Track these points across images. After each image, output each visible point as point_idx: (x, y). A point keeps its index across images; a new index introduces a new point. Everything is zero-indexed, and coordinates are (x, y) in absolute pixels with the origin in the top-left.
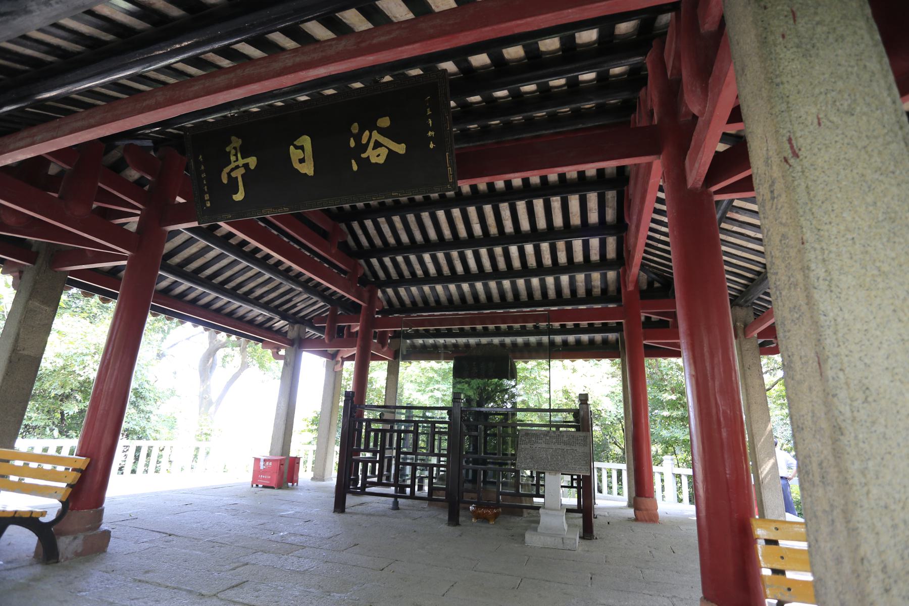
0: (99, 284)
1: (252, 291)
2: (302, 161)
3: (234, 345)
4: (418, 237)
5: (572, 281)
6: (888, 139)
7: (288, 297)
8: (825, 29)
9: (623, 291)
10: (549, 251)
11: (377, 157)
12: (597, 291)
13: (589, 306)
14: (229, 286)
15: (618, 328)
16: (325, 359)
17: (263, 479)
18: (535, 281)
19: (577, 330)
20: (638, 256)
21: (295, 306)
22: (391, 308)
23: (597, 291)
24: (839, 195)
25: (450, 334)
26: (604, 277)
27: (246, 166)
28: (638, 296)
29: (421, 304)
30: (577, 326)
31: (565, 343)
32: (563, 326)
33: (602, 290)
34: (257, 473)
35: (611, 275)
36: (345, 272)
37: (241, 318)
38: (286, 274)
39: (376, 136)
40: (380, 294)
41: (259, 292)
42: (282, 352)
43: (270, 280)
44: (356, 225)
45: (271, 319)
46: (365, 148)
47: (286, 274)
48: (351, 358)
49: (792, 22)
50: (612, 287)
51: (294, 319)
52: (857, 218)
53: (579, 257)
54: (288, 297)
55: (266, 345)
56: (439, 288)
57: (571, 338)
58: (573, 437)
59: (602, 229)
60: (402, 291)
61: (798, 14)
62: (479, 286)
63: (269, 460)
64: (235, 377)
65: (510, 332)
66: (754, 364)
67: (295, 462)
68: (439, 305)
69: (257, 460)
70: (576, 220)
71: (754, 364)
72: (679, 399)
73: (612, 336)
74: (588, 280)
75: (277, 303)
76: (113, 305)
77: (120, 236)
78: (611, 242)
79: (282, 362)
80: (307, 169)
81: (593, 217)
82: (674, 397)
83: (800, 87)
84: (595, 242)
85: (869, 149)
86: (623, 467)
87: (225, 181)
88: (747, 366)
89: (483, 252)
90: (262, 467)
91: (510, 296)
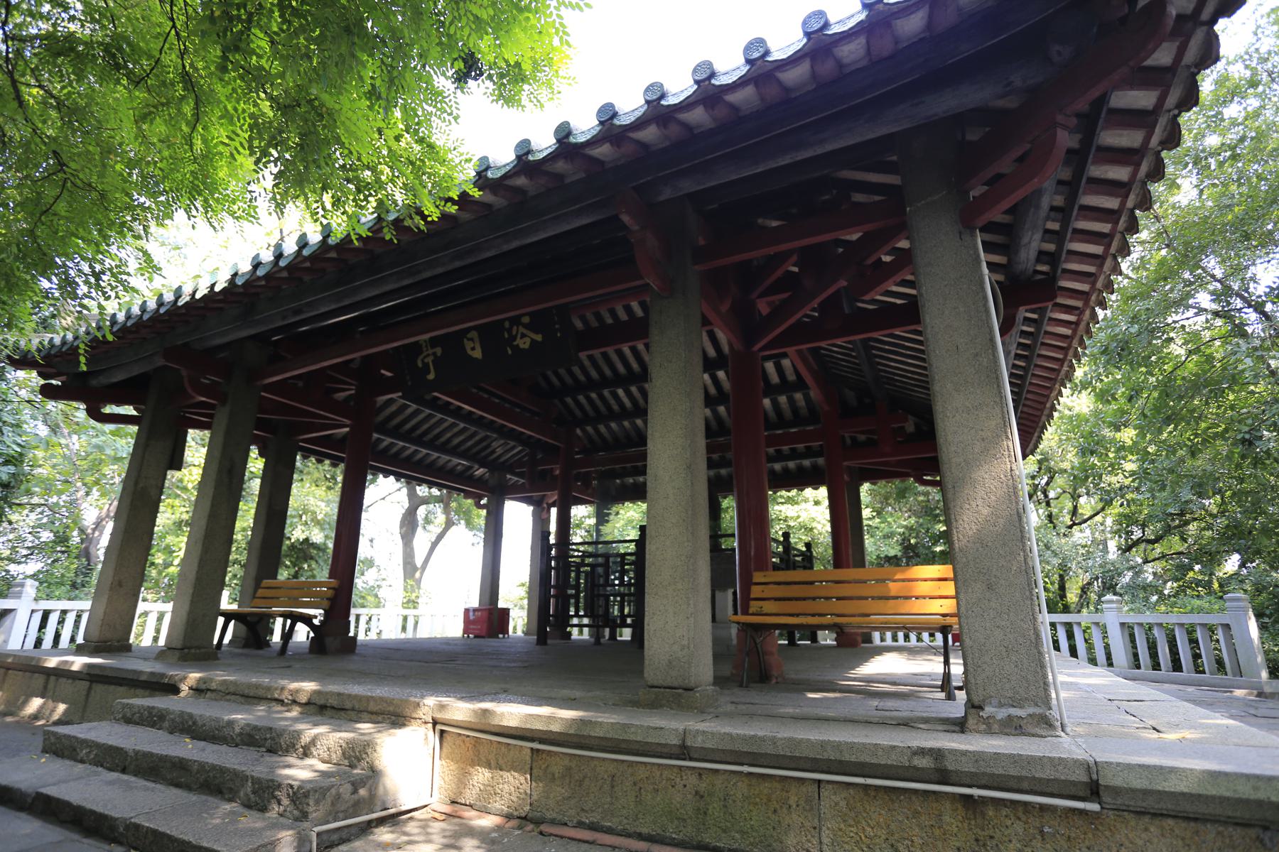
0: (324, 450)
1: (449, 440)
2: (473, 349)
3: (439, 500)
7: (484, 444)
11: (524, 344)
21: (493, 452)
27: (434, 354)
37: (442, 468)
38: (480, 422)
39: (522, 330)
40: (578, 431)
41: (456, 441)
42: (483, 502)
43: (465, 429)
45: (470, 468)
46: (515, 339)
47: (480, 422)
48: (553, 505)
51: (496, 466)
54: (484, 444)
55: (468, 495)
60: (602, 428)
64: (440, 537)
67: (505, 613)
75: (474, 450)
76: (342, 466)
77: (341, 408)
79: (484, 512)
80: (477, 354)
87: (420, 364)
90: (472, 617)
91: (788, 413)
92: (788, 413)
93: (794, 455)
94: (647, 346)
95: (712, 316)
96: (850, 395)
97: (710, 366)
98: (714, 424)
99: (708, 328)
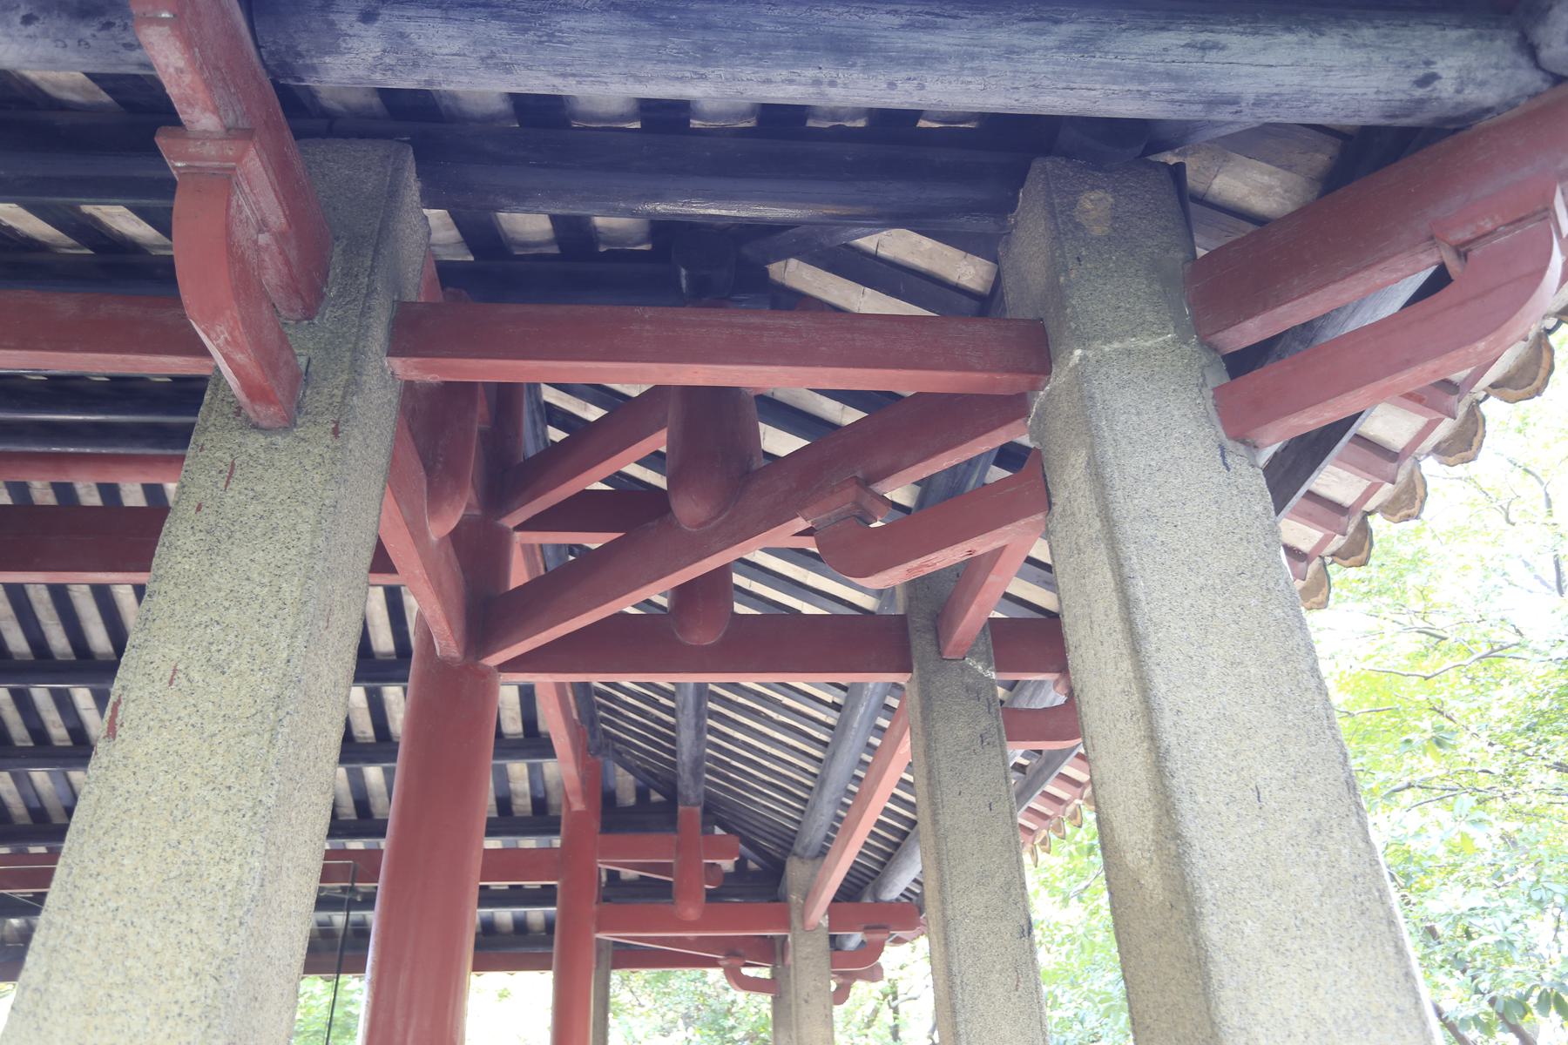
6: (251, 726)
8: (260, 508)
24: (135, 822)
49: (222, 485)
52: (140, 871)
61: (237, 473)
83: (177, 607)
85: (216, 740)
92: (522, 804)
93: (515, 897)
94: (140, 591)
95: (401, 549)
96: (625, 783)
97: (371, 668)
98: (348, 810)
99: (390, 579)
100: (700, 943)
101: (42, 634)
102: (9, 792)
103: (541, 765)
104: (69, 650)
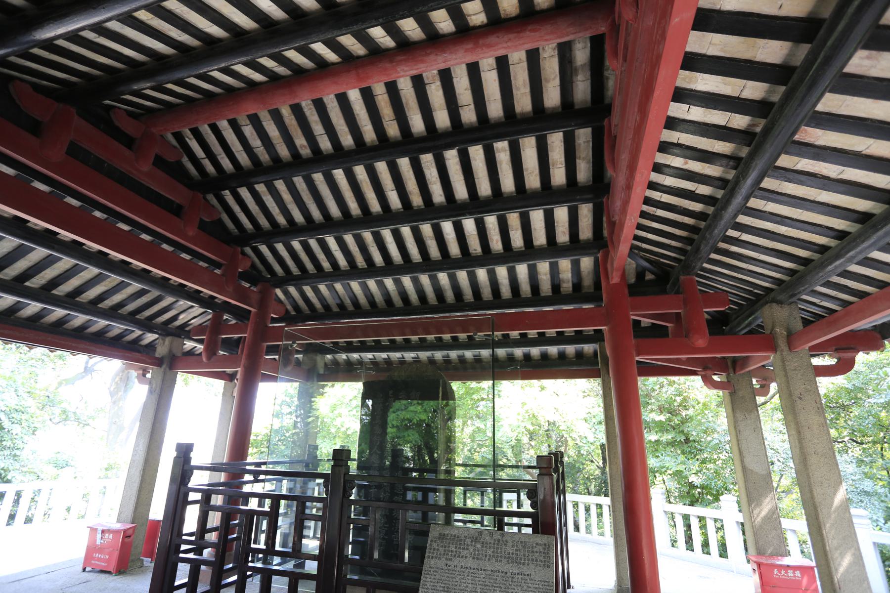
4: (316, 214)
5: (533, 273)
9: (603, 284)
10: (361, 101)
12: (567, 286)
13: (577, 306)
14: (35, 282)
15: (597, 337)
16: (223, 382)
17: (99, 559)
18: (482, 274)
19: (542, 340)
20: (629, 229)
22: (296, 316)
23: (567, 286)
25: (378, 347)
26: (576, 265)
28: (626, 291)
29: (351, 308)
30: (542, 335)
31: (527, 357)
32: (523, 335)
33: (574, 285)
34: (91, 550)
35: (587, 263)
36: (218, 265)
44: (227, 195)
50: (588, 281)
53: (540, 238)
56: (355, 285)
57: (535, 351)
58: (524, 544)
59: (572, 192)
62: (407, 281)
63: (110, 531)
65: (455, 344)
66: (807, 391)
68: (358, 310)
69: (93, 530)
70: (533, 181)
71: (807, 391)
72: (670, 420)
73: (588, 348)
74: (554, 270)
78: (586, 212)
81: (559, 176)
82: (663, 418)
84: (561, 214)
86: (606, 501)
88: (796, 393)
89: (406, 231)
90: (98, 542)
100: (689, 361)
101: (308, 210)
102: (849, 226)
103: (557, 262)
104: (321, 218)
